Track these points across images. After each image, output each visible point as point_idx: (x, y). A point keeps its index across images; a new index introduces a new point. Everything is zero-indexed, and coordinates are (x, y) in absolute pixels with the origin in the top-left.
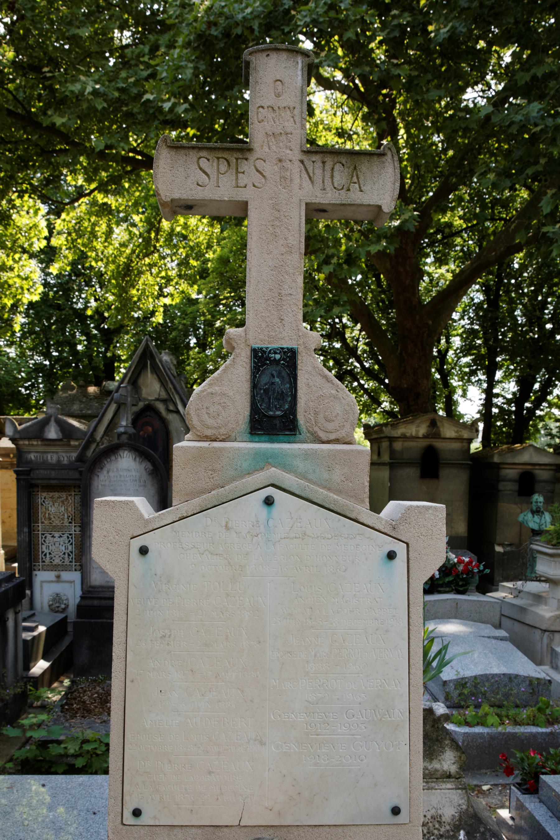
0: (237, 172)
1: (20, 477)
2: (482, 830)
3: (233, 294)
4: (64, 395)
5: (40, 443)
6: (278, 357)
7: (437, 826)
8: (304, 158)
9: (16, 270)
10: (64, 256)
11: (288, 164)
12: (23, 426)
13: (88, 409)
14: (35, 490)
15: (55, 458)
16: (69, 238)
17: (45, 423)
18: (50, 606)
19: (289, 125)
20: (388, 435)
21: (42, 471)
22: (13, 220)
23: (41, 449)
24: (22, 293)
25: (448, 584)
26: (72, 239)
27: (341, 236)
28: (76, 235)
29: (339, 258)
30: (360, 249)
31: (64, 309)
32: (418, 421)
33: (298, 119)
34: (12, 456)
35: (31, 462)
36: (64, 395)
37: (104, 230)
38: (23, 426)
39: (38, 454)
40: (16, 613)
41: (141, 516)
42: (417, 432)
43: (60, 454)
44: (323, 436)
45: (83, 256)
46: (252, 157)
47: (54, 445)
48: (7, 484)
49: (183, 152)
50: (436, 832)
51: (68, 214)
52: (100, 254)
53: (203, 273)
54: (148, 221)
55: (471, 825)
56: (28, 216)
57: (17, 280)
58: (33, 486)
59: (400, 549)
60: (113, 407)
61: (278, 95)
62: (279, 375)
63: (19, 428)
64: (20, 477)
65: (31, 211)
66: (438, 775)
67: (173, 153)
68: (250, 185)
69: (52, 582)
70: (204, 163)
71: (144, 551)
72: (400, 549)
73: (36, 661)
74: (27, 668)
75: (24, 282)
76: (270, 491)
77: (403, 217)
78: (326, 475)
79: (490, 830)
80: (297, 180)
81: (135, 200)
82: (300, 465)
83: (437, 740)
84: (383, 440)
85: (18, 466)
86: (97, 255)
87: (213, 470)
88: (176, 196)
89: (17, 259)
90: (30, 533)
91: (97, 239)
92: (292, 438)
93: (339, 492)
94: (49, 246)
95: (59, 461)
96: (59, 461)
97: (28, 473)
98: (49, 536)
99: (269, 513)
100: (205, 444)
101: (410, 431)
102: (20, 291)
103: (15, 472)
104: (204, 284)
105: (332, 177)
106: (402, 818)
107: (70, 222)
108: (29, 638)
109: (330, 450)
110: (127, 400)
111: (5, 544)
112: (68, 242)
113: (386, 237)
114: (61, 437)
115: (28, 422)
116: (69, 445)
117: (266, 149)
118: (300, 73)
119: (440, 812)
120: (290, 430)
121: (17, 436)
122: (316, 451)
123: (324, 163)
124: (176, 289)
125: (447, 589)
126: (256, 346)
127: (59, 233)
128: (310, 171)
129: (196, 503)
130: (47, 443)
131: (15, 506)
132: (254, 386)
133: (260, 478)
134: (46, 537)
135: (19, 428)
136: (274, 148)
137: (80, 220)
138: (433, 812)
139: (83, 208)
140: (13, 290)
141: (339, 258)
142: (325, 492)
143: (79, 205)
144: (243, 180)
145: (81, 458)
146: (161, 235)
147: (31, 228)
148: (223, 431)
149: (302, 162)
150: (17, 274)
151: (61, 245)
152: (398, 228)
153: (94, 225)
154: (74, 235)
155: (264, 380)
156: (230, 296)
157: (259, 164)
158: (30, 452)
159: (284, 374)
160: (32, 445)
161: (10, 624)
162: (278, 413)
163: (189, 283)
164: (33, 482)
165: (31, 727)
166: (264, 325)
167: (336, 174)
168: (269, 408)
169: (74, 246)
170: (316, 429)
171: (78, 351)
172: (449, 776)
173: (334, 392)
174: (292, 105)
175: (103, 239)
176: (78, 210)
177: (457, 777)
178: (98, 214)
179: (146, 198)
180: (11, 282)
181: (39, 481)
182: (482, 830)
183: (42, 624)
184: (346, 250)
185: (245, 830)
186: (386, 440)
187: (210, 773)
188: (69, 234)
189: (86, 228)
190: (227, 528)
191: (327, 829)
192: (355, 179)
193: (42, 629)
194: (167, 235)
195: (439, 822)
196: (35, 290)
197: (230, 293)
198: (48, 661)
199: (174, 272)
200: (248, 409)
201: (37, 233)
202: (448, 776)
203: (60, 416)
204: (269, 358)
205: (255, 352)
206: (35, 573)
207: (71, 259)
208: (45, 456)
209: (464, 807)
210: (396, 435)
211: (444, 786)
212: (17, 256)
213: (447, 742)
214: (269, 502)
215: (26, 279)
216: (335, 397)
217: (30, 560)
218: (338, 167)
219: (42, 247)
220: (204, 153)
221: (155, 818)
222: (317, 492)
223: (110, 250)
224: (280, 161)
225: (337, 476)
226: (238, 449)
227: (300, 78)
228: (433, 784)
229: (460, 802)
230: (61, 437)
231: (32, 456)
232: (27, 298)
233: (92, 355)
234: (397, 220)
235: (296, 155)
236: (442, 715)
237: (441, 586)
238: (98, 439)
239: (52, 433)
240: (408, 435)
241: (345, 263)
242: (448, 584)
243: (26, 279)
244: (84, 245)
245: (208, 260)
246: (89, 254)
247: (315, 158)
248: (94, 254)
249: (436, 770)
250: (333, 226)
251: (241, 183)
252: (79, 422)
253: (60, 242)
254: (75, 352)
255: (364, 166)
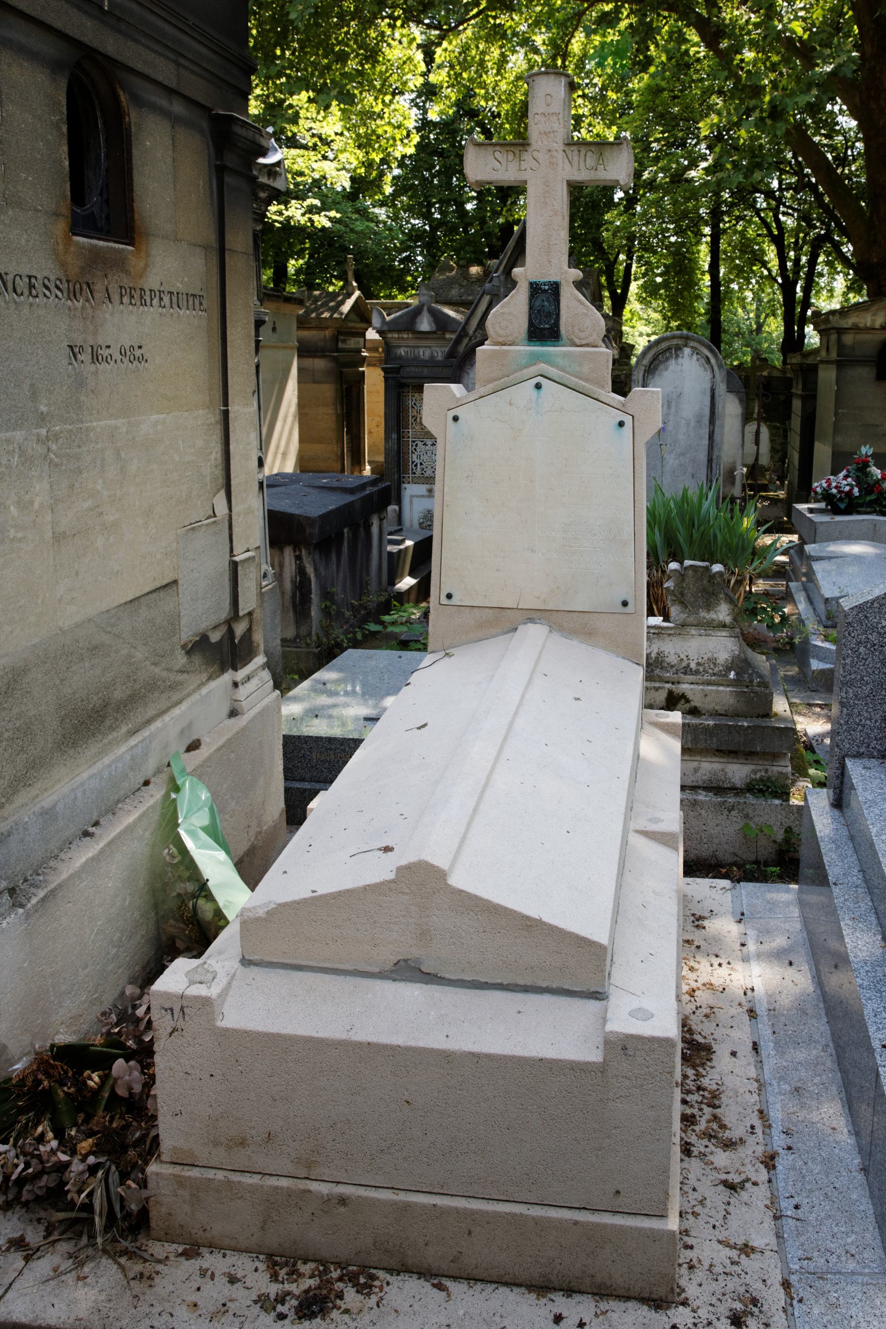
0: (520, 160)
1: (388, 376)
2: (750, 672)
3: (666, 135)
4: (441, 277)
5: (410, 336)
6: (547, 287)
7: (712, 666)
8: (566, 148)
9: (386, 116)
10: (445, 96)
11: (554, 153)
12: (392, 316)
13: (469, 295)
14: (406, 390)
15: (428, 353)
16: (452, 73)
17: (417, 312)
18: (420, 524)
19: (556, 126)
20: (836, 326)
21: (413, 369)
22: (382, 53)
23: (412, 343)
24: (394, 145)
25: (870, 504)
26: (455, 74)
27: (767, 83)
28: (461, 68)
29: (762, 111)
30: (787, 100)
31: (448, 157)
32: (874, 308)
33: (561, 121)
34: (381, 350)
35: (400, 358)
36: (441, 277)
37: (496, 60)
38: (392, 316)
39: (409, 349)
40: (381, 520)
41: (455, 395)
42: (873, 321)
43: (434, 348)
44: (578, 342)
45: (469, 94)
46: (530, 149)
47: (426, 338)
48: (375, 385)
49: (483, 147)
50: (710, 671)
51: (450, 43)
52: (490, 91)
53: (625, 108)
54: (552, 43)
55: (741, 668)
56: (400, 47)
57: (387, 128)
58: (402, 386)
59: (628, 420)
60: (486, 299)
61: (548, 105)
62: (548, 300)
63: (388, 318)
64: (388, 376)
65: (405, 40)
66: (715, 623)
67: (477, 148)
68: (529, 169)
69: (423, 496)
70: (497, 155)
71: (456, 419)
72: (628, 420)
73: (402, 577)
74: (392, 582)
75: (396, 131)
76: (539, 379)
77: (838, 60)
78: (578, 369)
79: (757, 673)
80: (561, 165)
81: (536, 17)
82: (561, 362)
83: (713, 594)
84: (832, 332)
85: (386, 363)
86: (487, 92)
87: (503, 365)
88: (479, 178)
89: (387, 101)
90: (399, 439)
91: (486, 73)
92: (556, 343)
93: (587, 380)
94: (426, 84)
95: (432, 356)
96: (432, 356)
97: (397, 370)
98: (420, 444)
99: (538, 394)
100: (497, 348)
101: (863, 321)
102: (391, 142)
103: (383, 369)
104: (627, 123)
105: (585, 160)
106: (630, 608)
107: (454, 52)
108: (395, 551)
109: (581, 352)
110: (499, 291)
111: (372, 459)
112: (450, 78)
113: (817, 85)
114: (434, 329)
115: (400, 309)
116: (445, 339)
117: (540, 143)
118: (563, 89)
119: (715, 655)
120: (555, 338)
121: (385, 328)
122: (571, 352)
123: (579, 151)
124: (590, 131)
125: (869, 510)
126: (532, 280)
127: (439, 67)
128: (570, 157)
129: (490, 387)
130: (419, 336)
131: (382, 413)
132: (531, 308)
133: (533, 370)
134: (416, 445)
135: (388, 318)
136: (545, 142)
137: (465, 49)
138: (709, 655)
139: (469, 33)
140: (383, 142)
141: (762, 111)
142: (576, 380)
143: (465, 29)
144: (524, 165)
145: (451, 354)
146: (570, 62)
147: (404, 63)
148: (510, 338)
149: (564, 151)
150: (387, 120)
151: (441, 82)
152: (833, 73)
153: (483, 53)
154: (458, 67)
155: (538, 303)
156: (663, 138)
157: (535, 154)
158: (400, 347)
159: (551, 299)
160: (402, 338)
161: (375, 530)
162: (547, 326)
163: (605, 124)
164: (403, 381)
165: (393, 623)
166: (538, 266)
167: (588, 159)
168: (540, 323)
169: (459, 83)
170: (573, 337)
171: (467, 212)
172: (724, 626)
173: (585, 311)
174: (557, 111)
175: (495, 71)
176: (463, 36)
177: (731, 627)
178: (489, 39)
179: (550, 14)
180: (380, 131)
181: (410, 380)
182: (750, 672)
183: (409, 539)
184: (770, 102)
185: (521, 612)
186: (834, 331)
187: (498, 570)
188: (452, 67)
189: (473, 58)
190: (510, 404)
191: (577, 614)
192: (601, 162)
193: (409, 543)
194: (578, 61)
195: (715, 664)
196: (410, 141)
197: (663, 132)
198: (415, 578)
199: (586, 109)
200: (527, 324)
201: (412, 67)
202: (724, 626)
203: (433, 305)
204: (540, 289)
205: (531, 284)
206: (404, 486)
207: (454, 99)
208: (416, 351)
209: (737, 653)
210: (845, 326)
211: (719, 634)
212: (388, 98)
213: (722, 596)
214: (538, 386)
215: (399, 127)
216: (586, 315)
217: (399, 471)
218: (589, 154)
219: (418, 85)
220: (498, 148)
221: (461, 600)
222: (570, 380)
223: (503, 86)
224: (549, 151)
225: (585, 369)
226: (519, 351)
227: (563, 92)
228: (710, 632)
229: (734, 648)
230: (434, 329)
231: (402, 351)
232: (399, 151)
233: (485, 216)
234: (831, 64)
235: (560, 147)
236: (717, 572)
237: (862, 505)
238: (471, 332)
239: (425, 324)
240: (861, 325)
241: (769, 117)
242: (870, 504)
243: (399, 127)
244: (470, 80)
245: (633, 91)
246: (477, 91)
247: (573, 148)
248: (483, 91)
249: (713, 620)
250: (756, 72)
251: (523, 168)
252: (455, 311)
253: (441, 78)
254: (462, 213)
255: (607, 152)
